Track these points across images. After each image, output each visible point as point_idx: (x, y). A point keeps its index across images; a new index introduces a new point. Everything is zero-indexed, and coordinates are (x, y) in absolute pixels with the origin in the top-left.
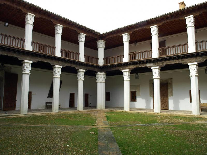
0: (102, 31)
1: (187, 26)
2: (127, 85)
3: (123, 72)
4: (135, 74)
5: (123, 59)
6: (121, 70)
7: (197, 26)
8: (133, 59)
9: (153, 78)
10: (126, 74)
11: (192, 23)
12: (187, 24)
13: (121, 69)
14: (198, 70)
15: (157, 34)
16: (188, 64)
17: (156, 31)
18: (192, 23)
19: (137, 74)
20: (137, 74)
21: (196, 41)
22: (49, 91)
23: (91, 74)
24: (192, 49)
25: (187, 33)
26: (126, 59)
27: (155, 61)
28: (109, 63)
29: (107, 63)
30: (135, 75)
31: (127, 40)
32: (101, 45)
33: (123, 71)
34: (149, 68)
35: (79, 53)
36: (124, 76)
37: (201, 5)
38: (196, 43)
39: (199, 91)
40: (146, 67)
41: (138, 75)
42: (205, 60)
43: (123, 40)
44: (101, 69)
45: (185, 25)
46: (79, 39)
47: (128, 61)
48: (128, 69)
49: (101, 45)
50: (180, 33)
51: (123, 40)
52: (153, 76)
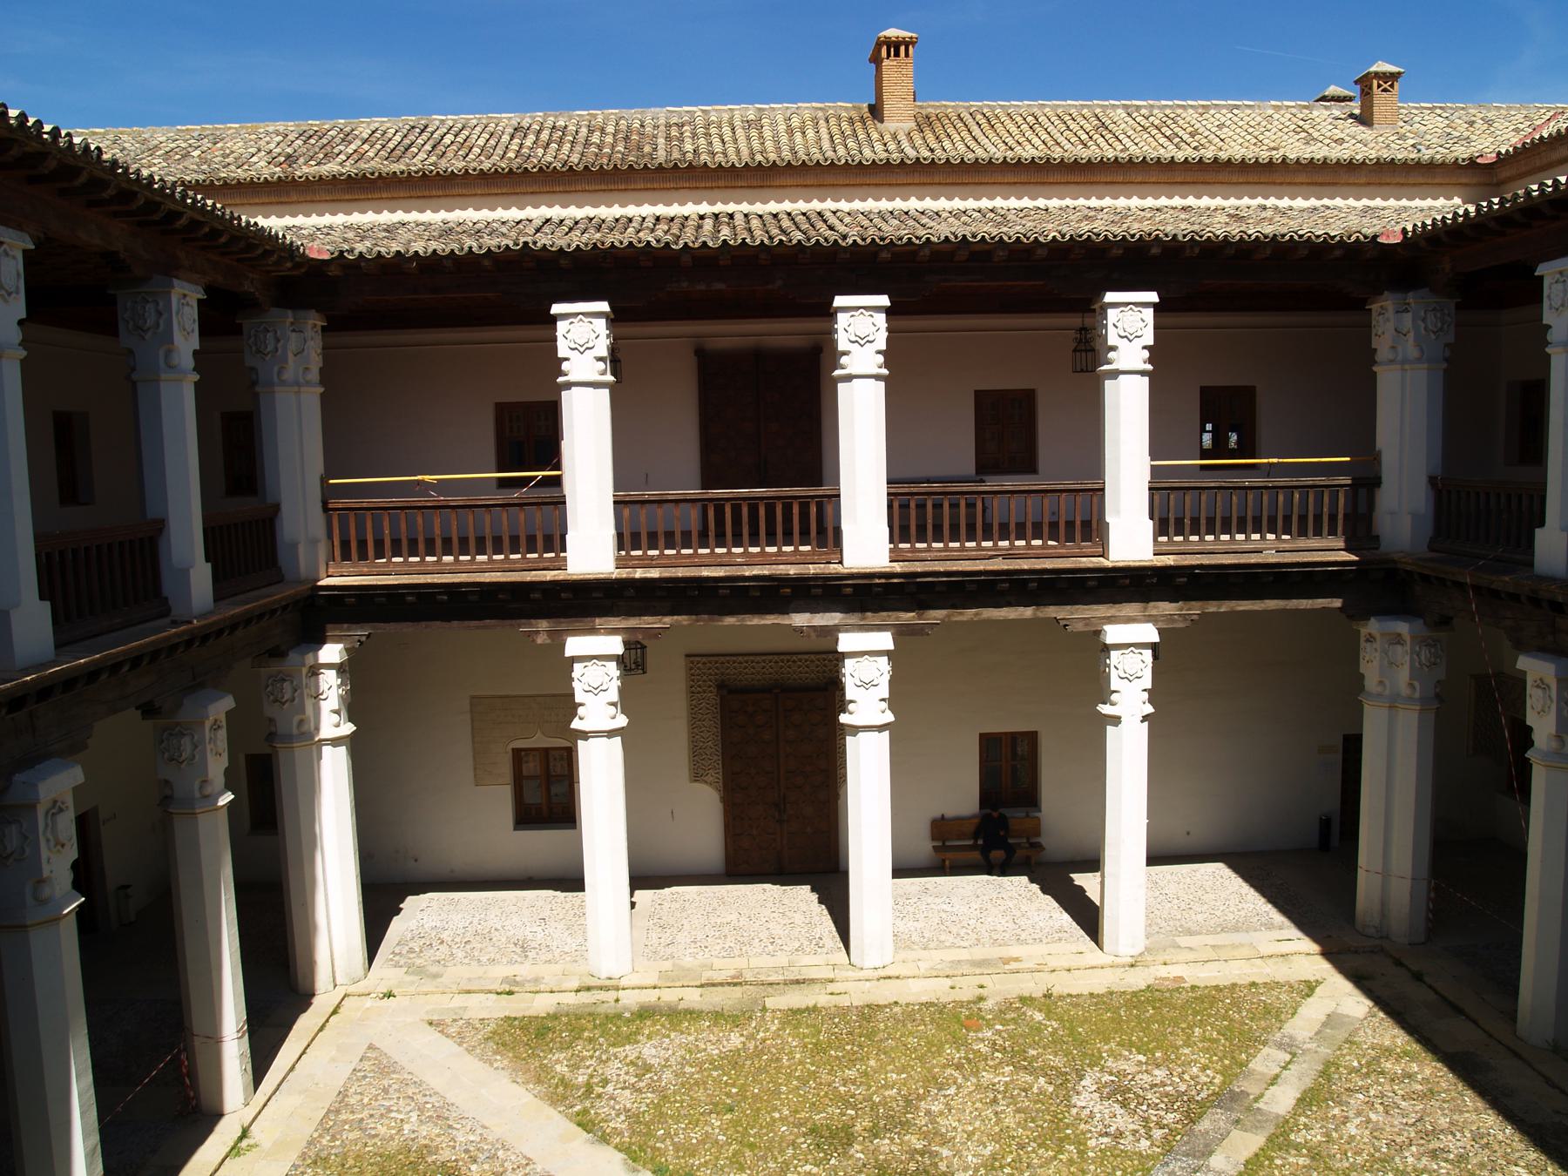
44: (866, 596)
48: (614, 631)
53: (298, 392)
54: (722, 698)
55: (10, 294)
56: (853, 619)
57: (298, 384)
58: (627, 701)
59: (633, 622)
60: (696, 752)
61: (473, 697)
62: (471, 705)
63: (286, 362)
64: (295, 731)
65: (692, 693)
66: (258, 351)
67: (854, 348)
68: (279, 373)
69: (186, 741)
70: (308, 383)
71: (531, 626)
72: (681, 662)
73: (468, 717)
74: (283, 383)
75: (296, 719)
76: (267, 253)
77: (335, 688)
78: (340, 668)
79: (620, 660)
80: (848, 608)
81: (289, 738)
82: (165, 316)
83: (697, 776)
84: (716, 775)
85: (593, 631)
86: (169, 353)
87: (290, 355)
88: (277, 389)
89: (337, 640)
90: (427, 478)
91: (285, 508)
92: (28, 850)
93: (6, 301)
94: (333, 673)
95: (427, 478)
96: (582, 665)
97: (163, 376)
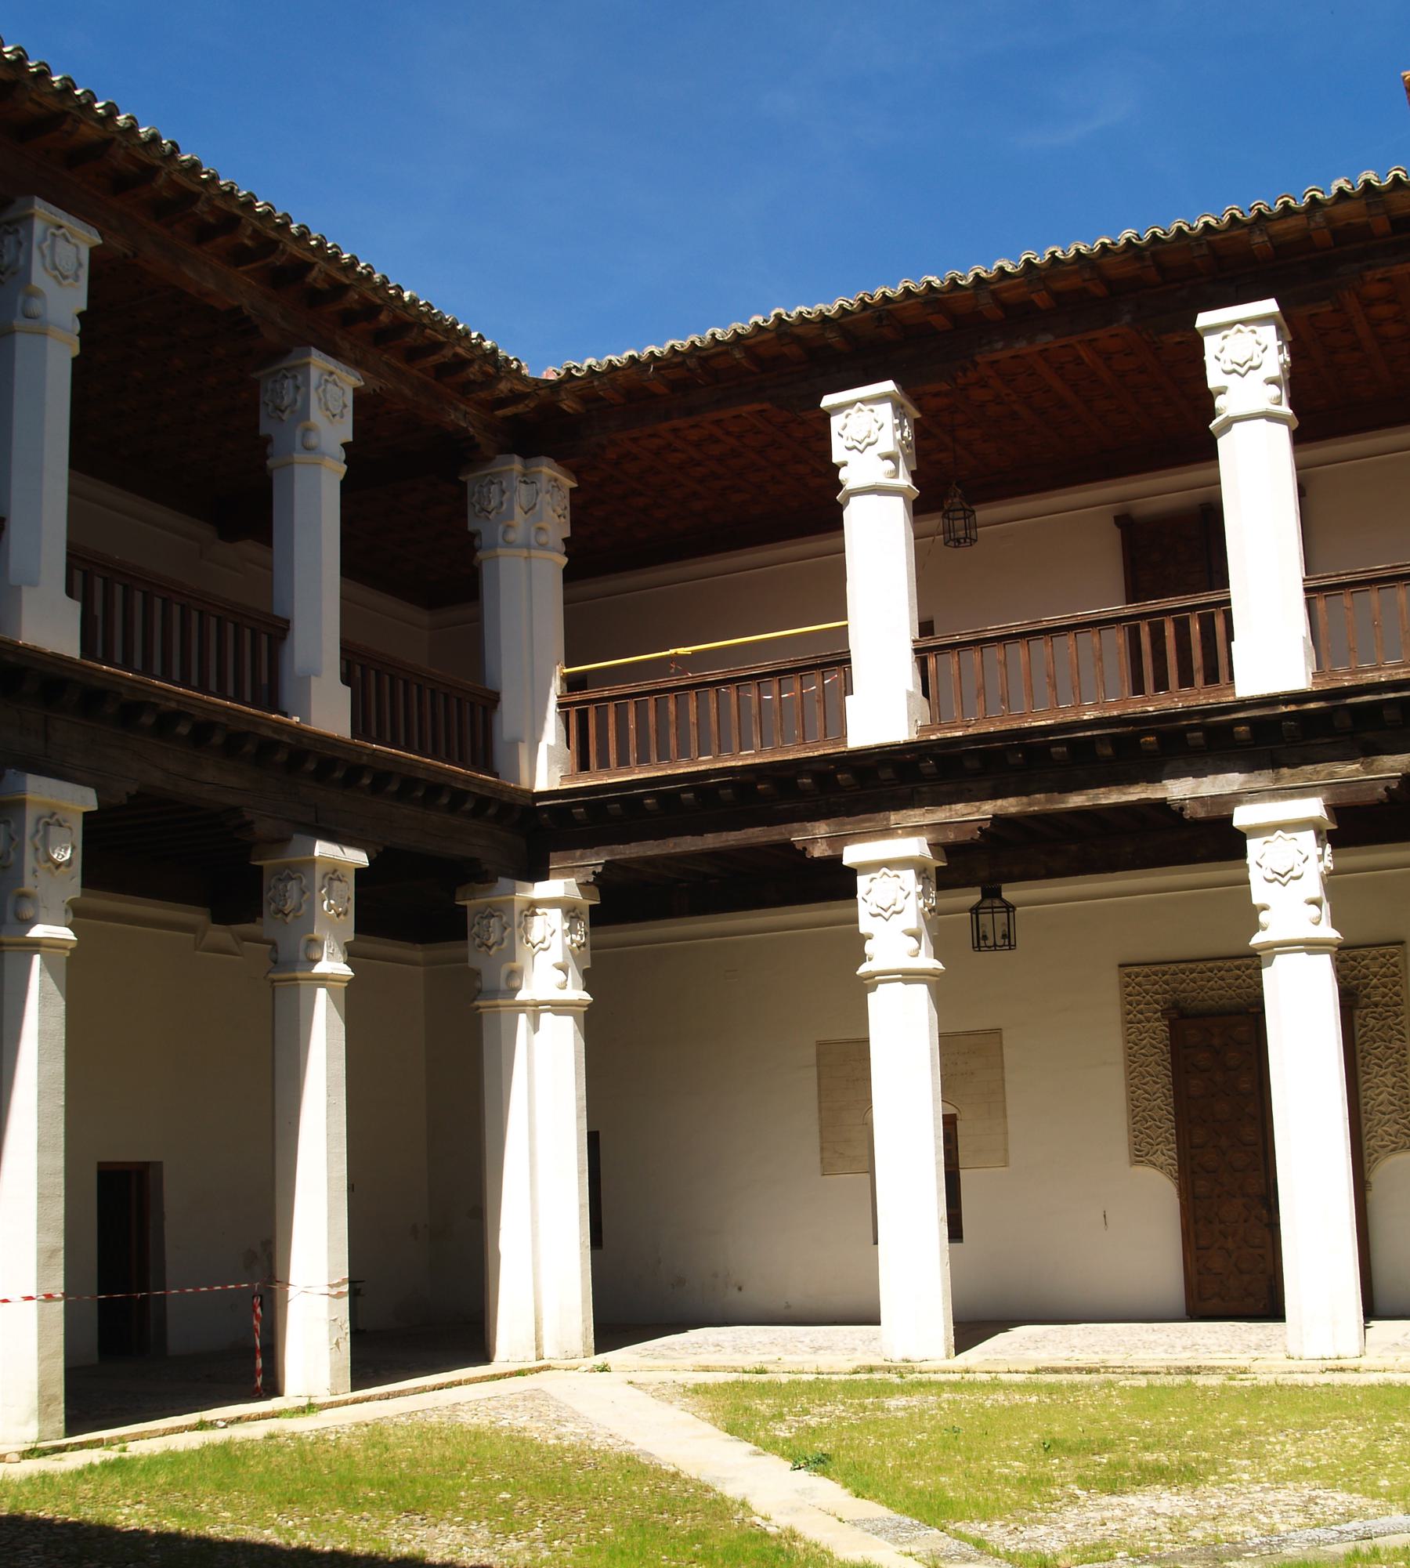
0: (545, 348)
1: (1212, 413)
2: (902, 1036)
3: (851, 874)
4: (973, 896)
5: (848, 699)
6: (819, 851)
7: (1319, 410)
8: (1186, 680)
9: (1257, 939)
10: (891, 887)
11: (1271, 381)
12: (1222, 391)
13: (815, 838)
14: (1332, 882)
15: (904, 481)
16: (1230, 818)
17: (1275, 372)
18: (1271, 381)
19: (997, 894)
20: (991, 893)
21: (926, 628)
22: (62, 1154)
23: (429, 916)
24: (882, 708)
25: (842, 550)
26: (882, 708)
27: (1277, 737)
28: (633, 756)
29: (633, 756)
30: (975, 910)
31: (889, 465)
32: (528, 527)
33: (851, 855)
34: (1197, 823)
35: (278, 611)
36: (865, 925)
37: (719, 349)
38: (927, 651)
39: (950, 1124)
40: (1162, 804)
41: (1009, 908)
42: (599, 869)
43: (836, 468)
44: (1277, 737)
45: (1203, 402)
46: (266, 427)
47: (914, 737)
48: (916, 830)
49: (528, 527)
50: (779, 540)
51: (836, 468)
52: (1250, 916)
53: (528, 558)
54: (1171, 1026)
55: (65, 277)
56: (1262, 780)
57: (528, 547)
58: (937, 930)
59: (941, 815)
60: (1138, 1116)
61: (820, 1044)
62: (819, 1054)
63: (512, 517)
64: (503, 986)
65: (1128, 1022)
66: (483, 510)
67: (1232, 381)
68: (505, 532)
69: (293, 887)
70: (543, 546)
71: (805, 831)
72: (1113, 977)
73: (814, 1072)
74: (509, 544)
75: (504, 970)
76: (462, 363)
77: (559, 934)
78: (571, 912)
79: (922, 873)
80: (1250, 765)
81: (495, 993)
82: (303, 389)
83: (1139, 1156)
84: (1167, 1154)
85: (887, 832)
86: (308, 430)
87: (518, 511)
88: (500, 551)
89: (564, 873)
90: (681, 651)
91: (504, 697)
92: (13, 856)
93: (60, 283)
94: (556, 914)
95: (681, 651)
96: (868, 877)
97: (297, 457)
